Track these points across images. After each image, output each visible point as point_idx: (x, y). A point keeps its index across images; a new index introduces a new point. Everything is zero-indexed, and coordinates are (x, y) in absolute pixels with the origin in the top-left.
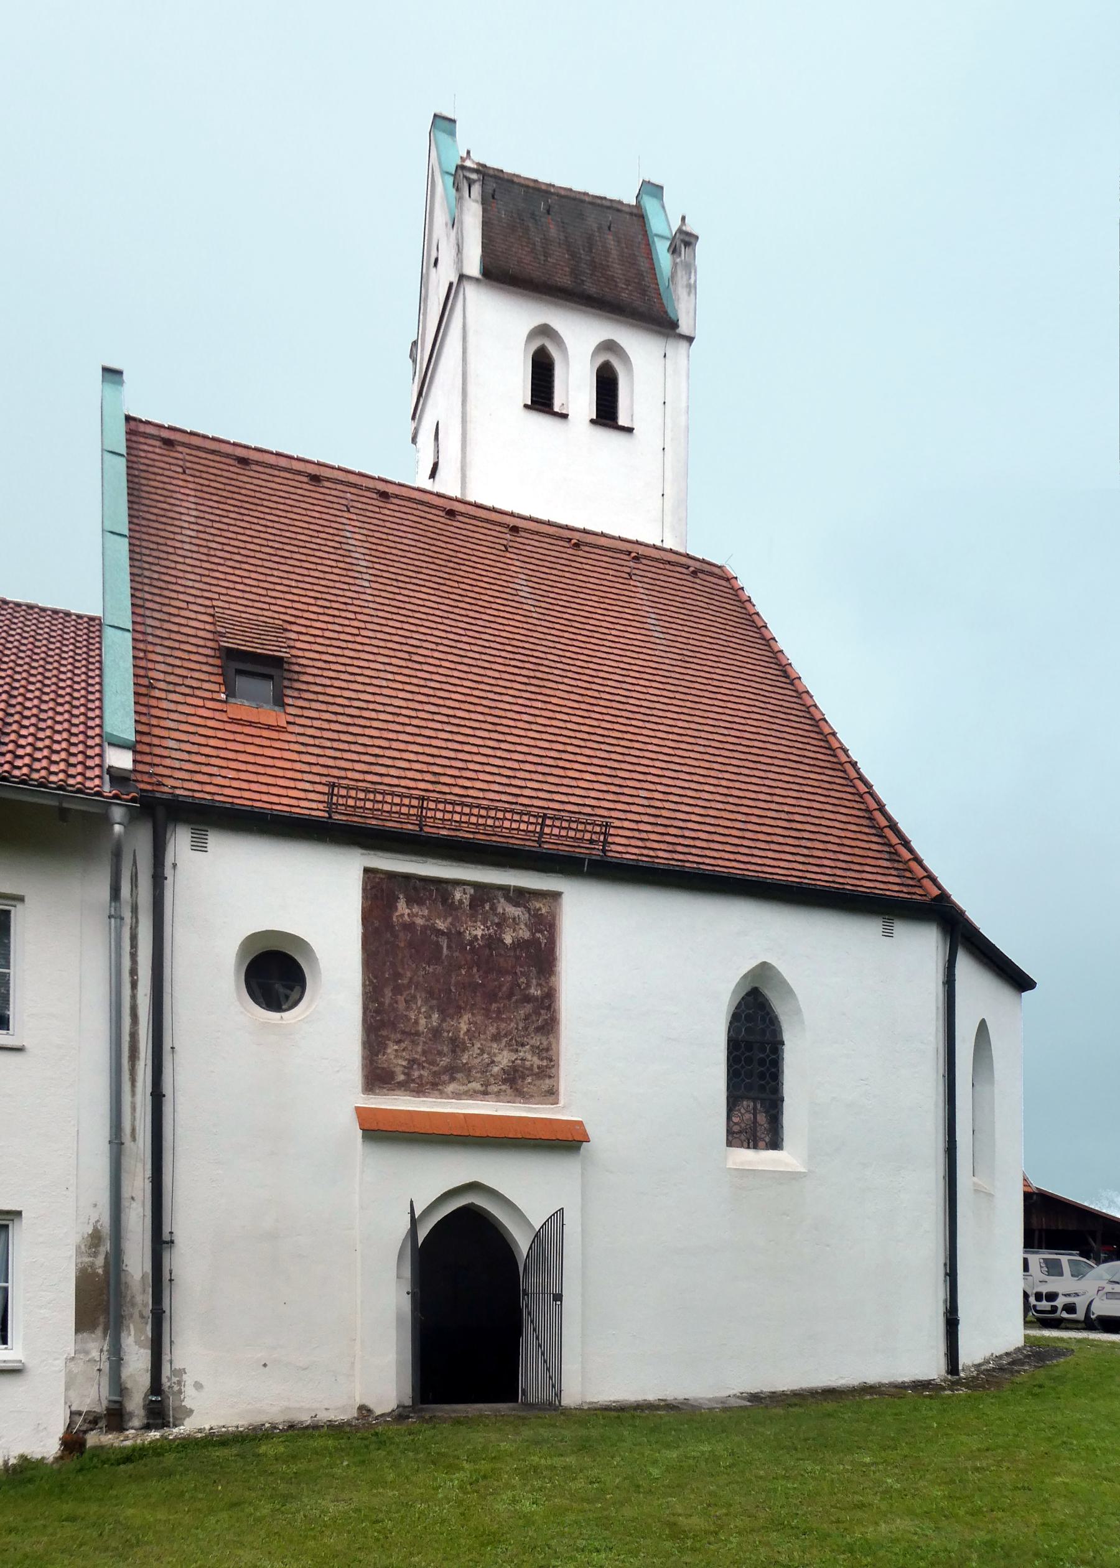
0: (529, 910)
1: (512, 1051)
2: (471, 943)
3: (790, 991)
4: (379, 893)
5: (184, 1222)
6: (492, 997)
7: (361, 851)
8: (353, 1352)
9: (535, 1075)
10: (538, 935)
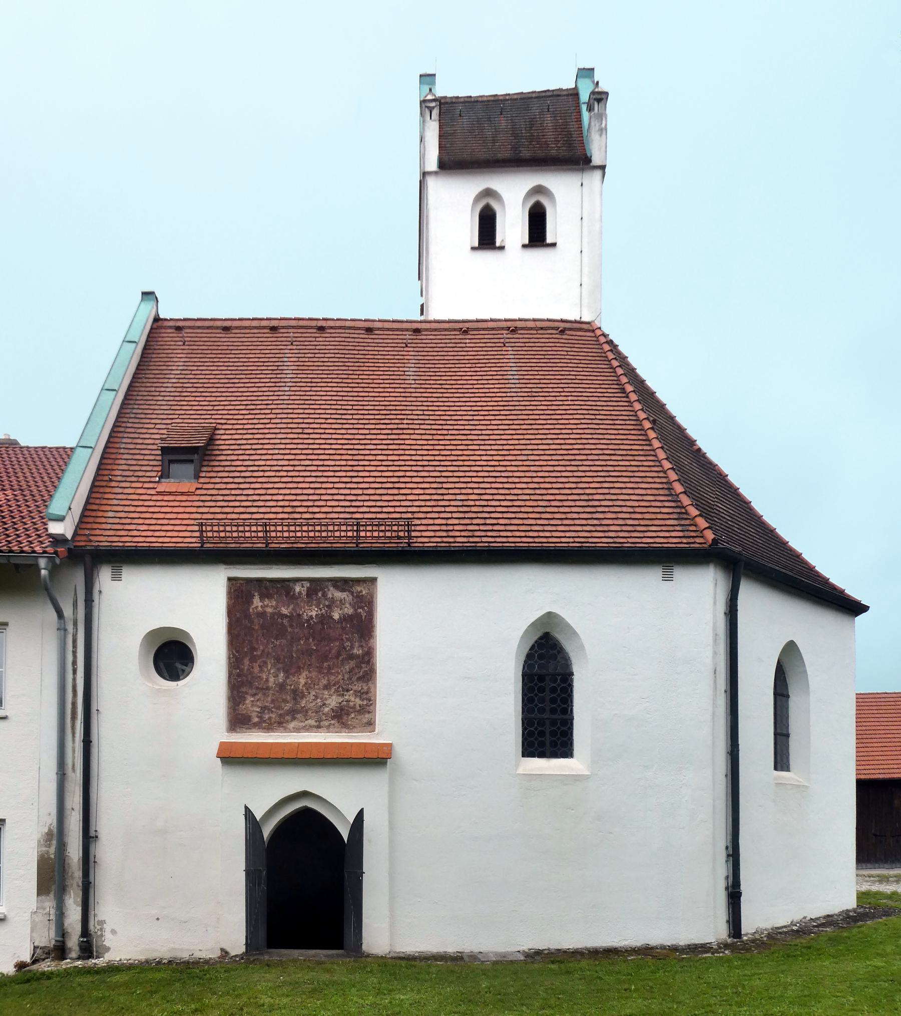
0: (352, 593)
1: (339, 695)
2: (308, 621)
3: (575, 633)
4: (239, 594)
5: (104, 824)
6: (325, 658)
7: (225, 566)
8: (211, 915)
9: (358, 710)
10: (359, 610)
